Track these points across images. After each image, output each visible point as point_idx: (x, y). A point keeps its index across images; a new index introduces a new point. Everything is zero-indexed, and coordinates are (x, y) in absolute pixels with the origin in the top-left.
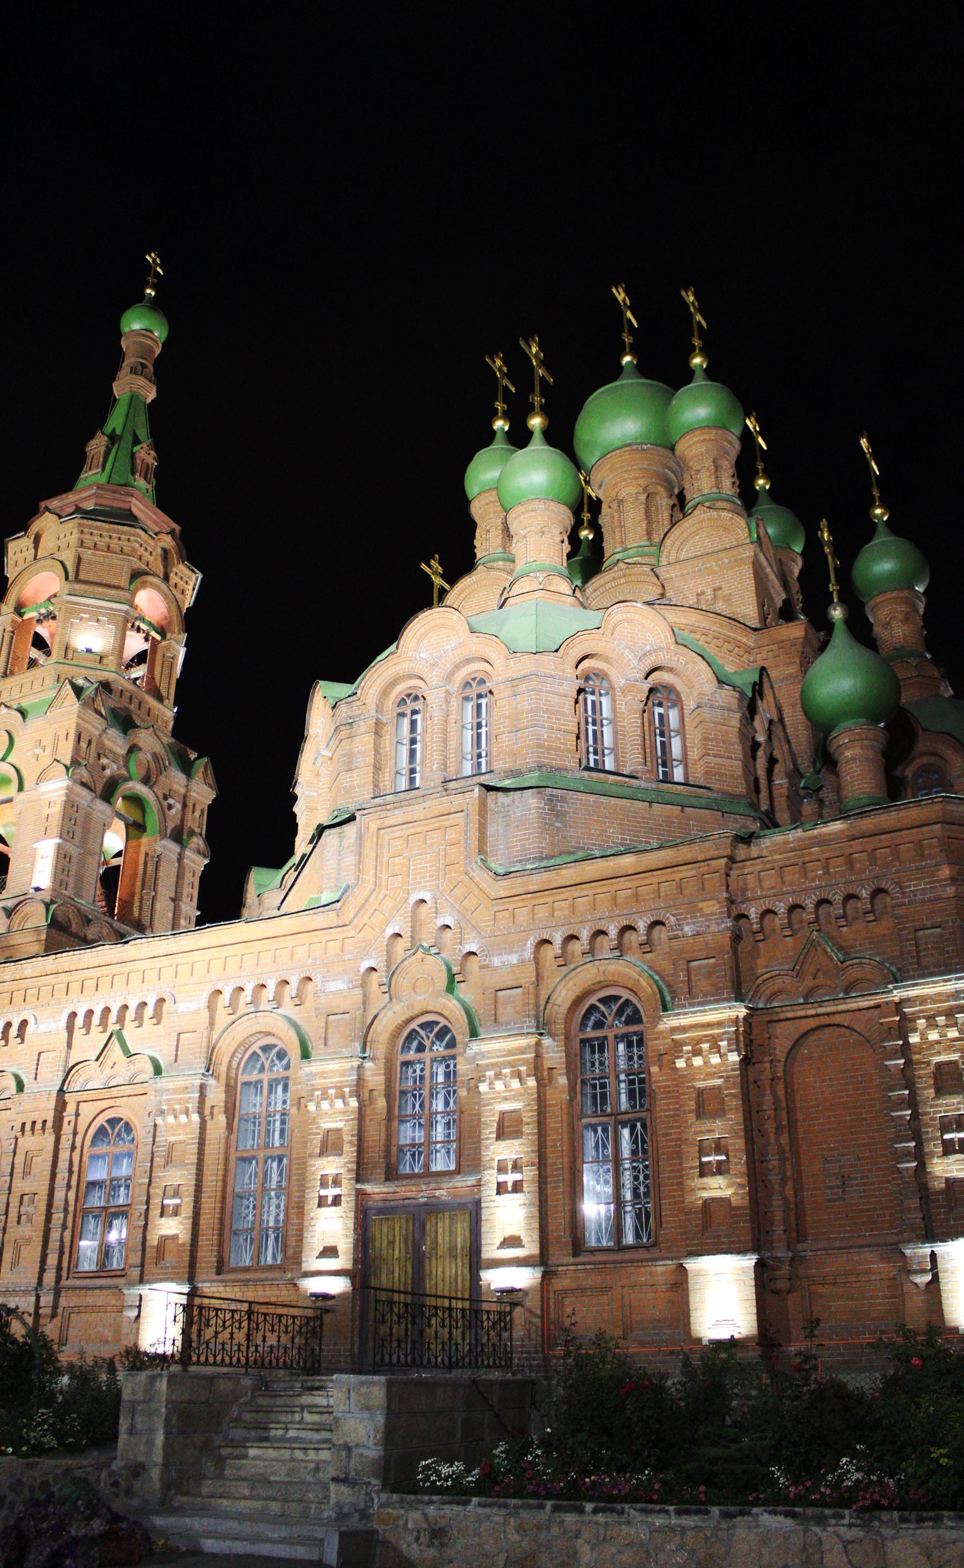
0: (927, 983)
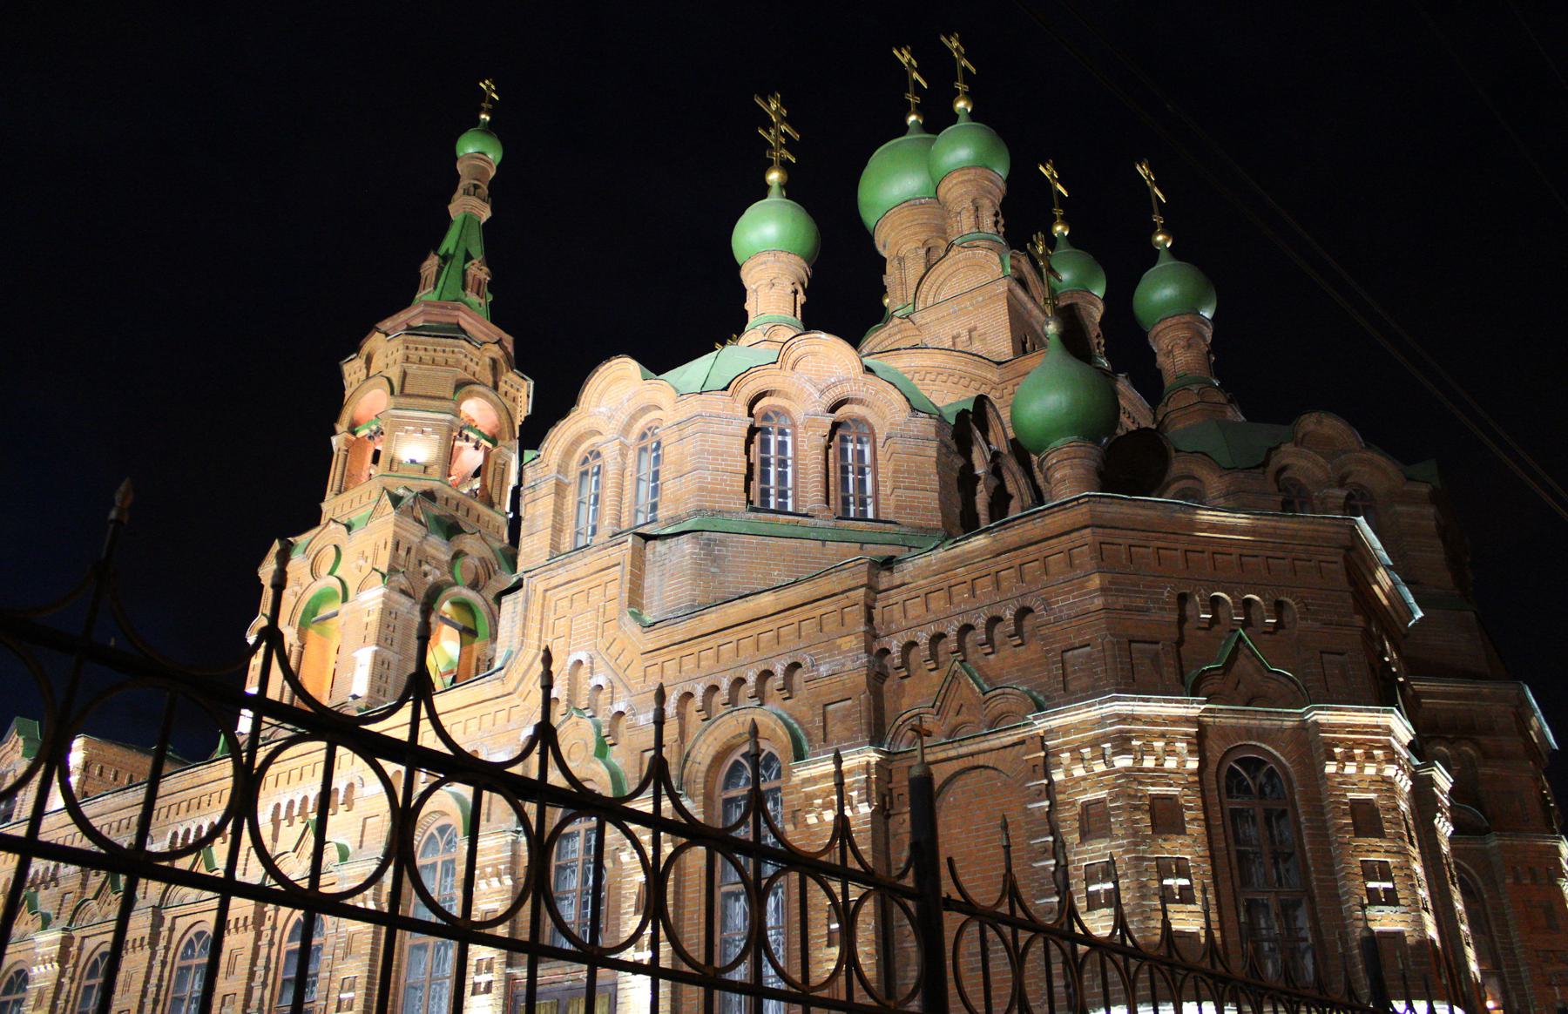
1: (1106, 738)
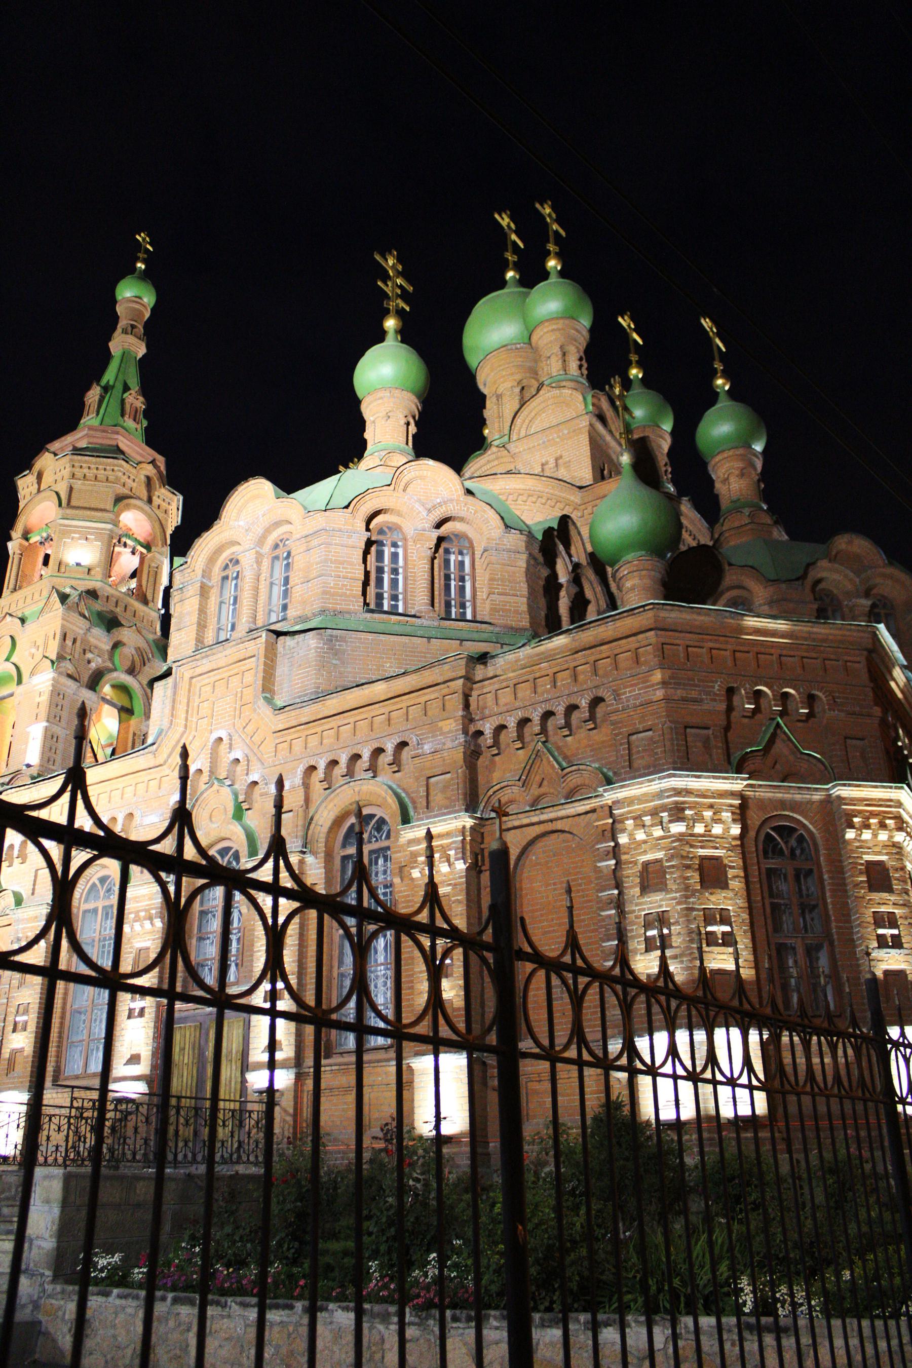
0: (633, 785)
1: (664, 808)
